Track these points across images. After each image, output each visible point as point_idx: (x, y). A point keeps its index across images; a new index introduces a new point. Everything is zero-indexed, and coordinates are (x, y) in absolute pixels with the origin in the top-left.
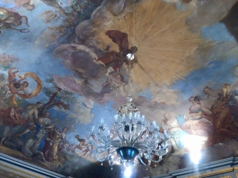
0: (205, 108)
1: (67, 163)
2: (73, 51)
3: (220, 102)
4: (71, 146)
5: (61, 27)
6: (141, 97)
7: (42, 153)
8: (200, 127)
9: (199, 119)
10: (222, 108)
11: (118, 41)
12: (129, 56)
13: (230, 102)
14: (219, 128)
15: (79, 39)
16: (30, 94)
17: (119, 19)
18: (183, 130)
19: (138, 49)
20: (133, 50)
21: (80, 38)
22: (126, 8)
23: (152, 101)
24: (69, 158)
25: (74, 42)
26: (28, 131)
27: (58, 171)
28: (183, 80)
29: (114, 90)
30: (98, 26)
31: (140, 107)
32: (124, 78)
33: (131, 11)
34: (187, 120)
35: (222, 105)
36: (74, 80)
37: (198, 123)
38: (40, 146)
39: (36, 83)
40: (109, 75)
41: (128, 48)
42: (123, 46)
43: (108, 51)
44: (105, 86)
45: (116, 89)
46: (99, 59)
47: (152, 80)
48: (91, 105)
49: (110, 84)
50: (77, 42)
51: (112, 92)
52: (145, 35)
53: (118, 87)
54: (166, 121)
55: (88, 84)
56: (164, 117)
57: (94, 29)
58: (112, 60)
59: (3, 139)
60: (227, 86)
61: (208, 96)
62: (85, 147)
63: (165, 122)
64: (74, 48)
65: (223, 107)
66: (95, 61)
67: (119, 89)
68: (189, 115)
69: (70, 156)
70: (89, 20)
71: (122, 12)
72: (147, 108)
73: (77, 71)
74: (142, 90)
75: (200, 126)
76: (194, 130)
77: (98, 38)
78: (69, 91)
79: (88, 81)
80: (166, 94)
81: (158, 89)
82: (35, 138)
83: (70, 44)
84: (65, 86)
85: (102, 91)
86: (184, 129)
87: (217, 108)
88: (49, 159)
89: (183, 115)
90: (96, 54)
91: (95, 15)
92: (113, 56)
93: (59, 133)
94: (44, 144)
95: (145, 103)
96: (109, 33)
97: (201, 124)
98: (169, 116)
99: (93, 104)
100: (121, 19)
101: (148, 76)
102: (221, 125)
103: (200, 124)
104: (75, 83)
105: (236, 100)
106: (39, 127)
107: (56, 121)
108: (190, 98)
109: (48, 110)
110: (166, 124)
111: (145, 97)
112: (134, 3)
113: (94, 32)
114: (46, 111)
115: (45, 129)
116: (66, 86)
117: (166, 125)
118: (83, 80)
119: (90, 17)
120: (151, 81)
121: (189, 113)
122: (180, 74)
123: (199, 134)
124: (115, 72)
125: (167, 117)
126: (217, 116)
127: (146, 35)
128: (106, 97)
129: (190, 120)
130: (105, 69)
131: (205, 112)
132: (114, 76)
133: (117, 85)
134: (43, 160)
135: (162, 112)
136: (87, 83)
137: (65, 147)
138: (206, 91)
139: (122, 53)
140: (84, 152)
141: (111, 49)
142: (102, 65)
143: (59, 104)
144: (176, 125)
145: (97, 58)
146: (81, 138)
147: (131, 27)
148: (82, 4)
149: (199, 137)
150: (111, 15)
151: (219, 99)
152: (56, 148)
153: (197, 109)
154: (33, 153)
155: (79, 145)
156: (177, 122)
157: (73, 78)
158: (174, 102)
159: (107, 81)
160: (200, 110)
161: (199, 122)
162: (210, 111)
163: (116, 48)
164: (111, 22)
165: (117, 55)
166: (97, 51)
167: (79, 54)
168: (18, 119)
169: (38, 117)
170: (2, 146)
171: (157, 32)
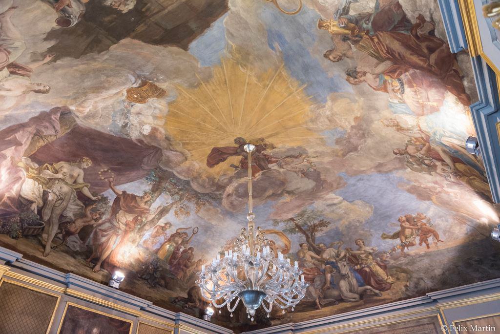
0: (376, 67)
1: (415, 275)
4: (394, 252)
5: (197, 203)
7: (369, 287)
9: (402, 85)
11: (225, 156)
16: (286, 246)
19: (239, 136)
20: (241, 143)
22: (177, 149)
24: (410, 268)
26: (329, 275)
27: (410, 294)
29: (315, 168)
38: (358, 281)
39: (274, 235)
42: (232, 152)
48: (337, 198)
59: (317, 301)
61: (348, 57)
62: (415, 238)
65: (376, 40)
67: (314, 163)
69: (407, 264)
70: (191, 182)
71: (182, 154)
72: (365, 141)
73: (269, 197)
78: (298, 212)
82: (344, 277)
88: (385, 288)
89: (389, 101)
91: (184, 176)
93: (359, 252)
94: (359, 276)
100: (191, 153)
102: (422, 58)
103: (415, 88)
104: (288, 202)
105: (359, 14)
106: (332, 264)
107: (338, 243)
108: (350, 83)
109: (317, 242)
113: (207, 177)
114: (317, 245)
115: (341, 260)
117: (411, 132)
121: (385, 93)
127: (217, 128)
133: (305, 163)
134: (377, 294)
137: (388, 259)
140: (424, 244)
143: (314, 229)
146: (392, 234)
147: (204, 143)
148: (169, 187)
151: (356, 42)
152: (380, 271)
154: (357, 294)
155: (402, 242)
161: (411, 86)
164: (195, 163)
168: (308, 273)
169: (319, 256)
170: (323, 309)
171: (212, 118)
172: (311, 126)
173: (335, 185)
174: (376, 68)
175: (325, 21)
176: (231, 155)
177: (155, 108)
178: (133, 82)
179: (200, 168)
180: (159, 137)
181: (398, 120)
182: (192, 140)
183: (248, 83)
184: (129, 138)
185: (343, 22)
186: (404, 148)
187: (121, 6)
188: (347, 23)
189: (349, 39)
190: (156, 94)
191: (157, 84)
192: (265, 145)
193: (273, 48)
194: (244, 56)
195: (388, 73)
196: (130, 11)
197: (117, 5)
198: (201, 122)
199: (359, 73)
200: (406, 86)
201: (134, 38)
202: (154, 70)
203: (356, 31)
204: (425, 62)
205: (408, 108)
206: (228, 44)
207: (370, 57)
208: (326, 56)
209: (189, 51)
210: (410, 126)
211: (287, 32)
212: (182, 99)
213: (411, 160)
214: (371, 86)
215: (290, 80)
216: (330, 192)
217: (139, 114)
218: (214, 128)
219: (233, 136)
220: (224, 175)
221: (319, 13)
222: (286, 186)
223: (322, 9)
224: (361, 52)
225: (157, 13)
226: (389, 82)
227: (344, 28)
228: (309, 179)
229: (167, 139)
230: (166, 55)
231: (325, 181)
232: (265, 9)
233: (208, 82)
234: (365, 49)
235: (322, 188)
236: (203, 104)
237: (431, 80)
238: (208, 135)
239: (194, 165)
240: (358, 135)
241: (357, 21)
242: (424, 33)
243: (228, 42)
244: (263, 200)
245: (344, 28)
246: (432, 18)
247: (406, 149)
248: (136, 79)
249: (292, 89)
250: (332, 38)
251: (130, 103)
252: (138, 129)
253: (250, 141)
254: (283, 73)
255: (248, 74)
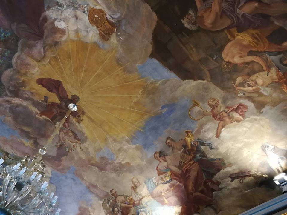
0: (173, 166)
2: (9, 106)
3: (187, 155)
6: (102, 158)
8: (172, 193)
9: (169, 182)
10: (190, 164)
12: (71, 105)
13: (198, 155)
14: (192, 192)
15: (11, 92)
17: (45, 66)
18: (155, 200)
19: (80, 97)
21: (10, 90)
22: (47, 53)
23: (116, 162)
25: (7, 95)
28: (140, 131)
29: (70, 151)
30: (25, 74)
31: (105, 172)
32: (77, 135)
33: (54, 55)
34: (156, 184)
35: (189, 159)
36: (22, 141)
37: (169, 187)
40: (60, 132)
41: (68, 97)
42: (61, 95)
43: (48, 103)
44: (59, 147)
45: (73, 150)
46: (42, 113)
47: (108, 133)
48: (49, 173)
49: (65, 144)
50: (9, 94)
51: (69, 153)
52: (80, 81)
53: (74, 147)
54: (136, 189)
55: (39, 145)
56: (132, 183)
57: (22, 78)
58: (56, 114)
60: (189, 134)
61: (172, 150)
63: (135, 189)
64: (9, 102)
65: (191, 163)
66: (37, 116)
67: (75, 149)
68: (158, 178)
70: (12, 69)
71: (44, 57)
72: (112, 173)
73: (22, 130)
74: (101, 149)
75: (172, 191)
76: (166, 198)
77: (32, 89)
78: (19, 155)
79: (38, 141)
80: (130, 153)
81: (118, 146)
83: (3, 97)
84: (12, 149)
85: (57, 154)
86: (156, 197)
87: (186, 164)
89: (152, 178)
90: (36, 107)
91: (16, 63)
92: (55, 108)
95: (109, 165)
96: (40, 82)
97: (173, 188)
98: (138, 182)
99: (51, 172)
100: (47, 64)
101: (102, 130)
102: (194, 188)
103: (171, 189)
104: (24, 144)
105: (204, 151)
108: (155, 154)
110: (136, 193)
111: (107, 157)
112: (53, 46)
116: (14, 149)
117: (136, 195)
118: (32, 141)
119: (12, 65)
120: (108, 136)
121: (157, 175)
122: (136, 124)
123: (172, 204)
124: (64, 128)
125: (136, 183)
126: (187, 175)
127: (82, 81)
128: (65, 162)
129: (160, 184)
130: (52, 125)
131: (174, 171)
132: (66, 133)
133: (72, 145)
135: (130, 176)
136: (38, 145)
138: (169, 143)
139: (64, 104)
141: (50, 100)
142: (48, 121)
144: (146, 192)
145: (38, 112)
149: (171, 207)
150: (33, 61)
151: (185, 152)
153: (165, 168)
156: (147, 189)
157: (19, 139)
158: (138, 161)
159: (60, 140)
160: (168, 168)
161: (171, 187)
162: (179, 170)
163: (54, 98)
165: (59, 106)
166: (36, 104)
167: (17, 108)
172: (110, 140)
173: (60, 167)
174: (172, 166)
175: (192, 134)
176: (58, 95)
177: (87, 31)
178: (113, 16)
179: (33, 74)
180: (56, 36)
181: (140, 186)
182: (62, 63)
183: (131, 96)
184: (46, 9)
185: (195, 144)
186: (119, 194)
187: (188, 20)
188: (195, 146)
189: (185, 148)
190: (103, 33)
191: (114, 35)
192: (79, 116)
193: (162, 108)
194: (151, 91)
195: (173, 173)
196: (183, 25)
197: (189, 17)
198: (84, 68)
199: (165, 158)
200: (169, 184)
201: (157, 22)
202: (128, 34)
203: (192, 152)
204: (192, 189)
205: (153, 189)
206: (158, 81)
207: (179, 162)
208: (168, 138)
209: (149, 58)
210: (140, 193)
211: (178, 113)
212: (103, 53)
213: (111, 201)
214: (158, 166)
215: (142, 121)
216: (53, 168)
217: (77, 17)
218: (81, 79)
219: (79, 93)
220: (33, 94)
221: (195, 130)
222: (41, 138)
223: (198, 132)
224: (180, 156)
225: (181, 42)
226: (166, 175)
227: (191, 144)
228: (58, 151)
229: (56, 43)
230: (144, 41)
231: (61, 161)
232: (188, 100)
233: (124, 71)
234: (183, 158)
235: (53, 161)
236: (102, 69)
237: (183, 196)
238: (73, 75)
239: (34, 69)
240: (115, 168)
241: (198, 150)
242: (210, 186)
243: (159, 81)
244: (15, 127)
245: (191, 144)
246: (222, 188)
247: (119, 196)
248: (116, 19)
249: (136, 124)
250: (182, 139)
251: (87, 10)
252: (59, 17)
253: (79, 106)
254: (146, 116)
255: (138, 96)
